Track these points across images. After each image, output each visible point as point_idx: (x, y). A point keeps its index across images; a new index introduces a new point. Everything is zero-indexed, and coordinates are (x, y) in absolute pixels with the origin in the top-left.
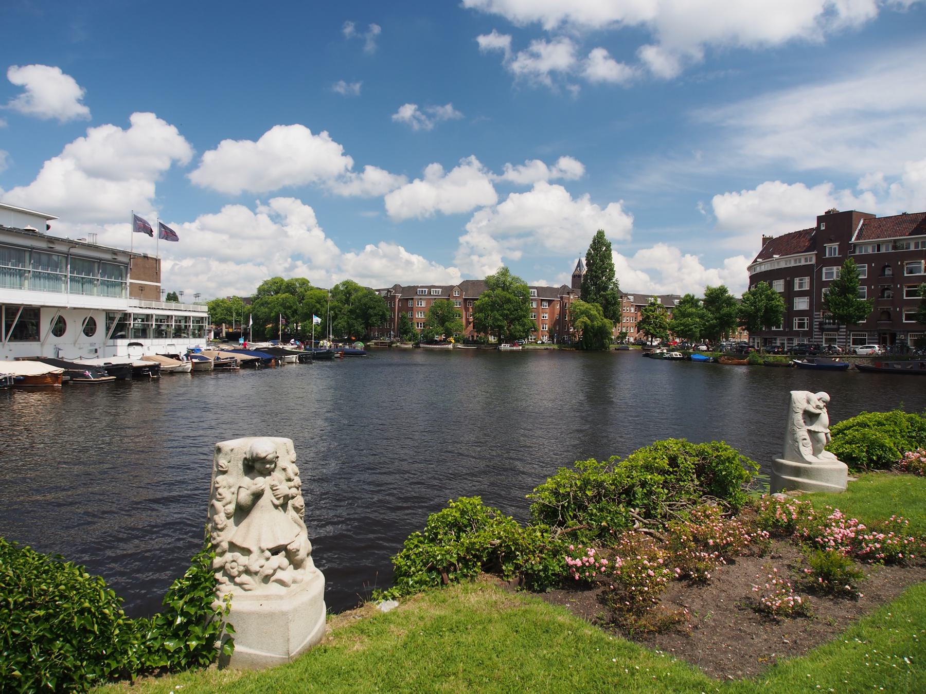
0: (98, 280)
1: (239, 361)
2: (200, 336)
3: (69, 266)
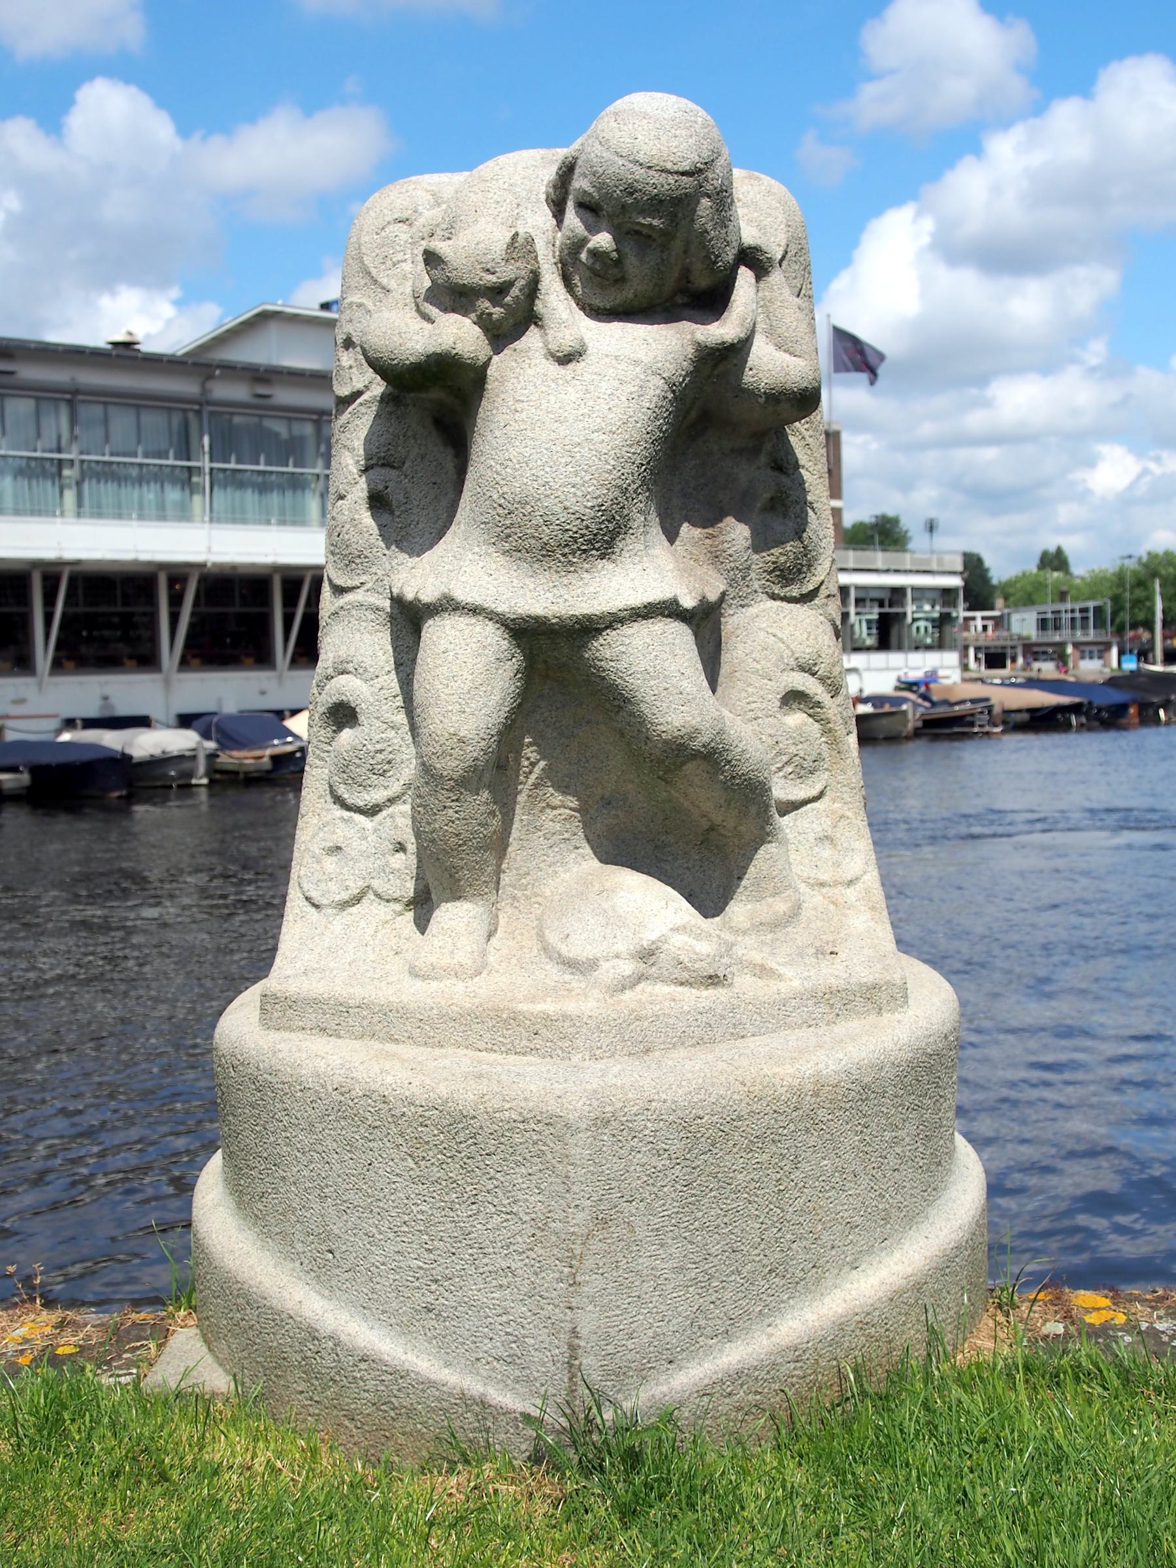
0: (72, 462)
1: (997, 710)
2: (940, 645)
3: (206, 440)
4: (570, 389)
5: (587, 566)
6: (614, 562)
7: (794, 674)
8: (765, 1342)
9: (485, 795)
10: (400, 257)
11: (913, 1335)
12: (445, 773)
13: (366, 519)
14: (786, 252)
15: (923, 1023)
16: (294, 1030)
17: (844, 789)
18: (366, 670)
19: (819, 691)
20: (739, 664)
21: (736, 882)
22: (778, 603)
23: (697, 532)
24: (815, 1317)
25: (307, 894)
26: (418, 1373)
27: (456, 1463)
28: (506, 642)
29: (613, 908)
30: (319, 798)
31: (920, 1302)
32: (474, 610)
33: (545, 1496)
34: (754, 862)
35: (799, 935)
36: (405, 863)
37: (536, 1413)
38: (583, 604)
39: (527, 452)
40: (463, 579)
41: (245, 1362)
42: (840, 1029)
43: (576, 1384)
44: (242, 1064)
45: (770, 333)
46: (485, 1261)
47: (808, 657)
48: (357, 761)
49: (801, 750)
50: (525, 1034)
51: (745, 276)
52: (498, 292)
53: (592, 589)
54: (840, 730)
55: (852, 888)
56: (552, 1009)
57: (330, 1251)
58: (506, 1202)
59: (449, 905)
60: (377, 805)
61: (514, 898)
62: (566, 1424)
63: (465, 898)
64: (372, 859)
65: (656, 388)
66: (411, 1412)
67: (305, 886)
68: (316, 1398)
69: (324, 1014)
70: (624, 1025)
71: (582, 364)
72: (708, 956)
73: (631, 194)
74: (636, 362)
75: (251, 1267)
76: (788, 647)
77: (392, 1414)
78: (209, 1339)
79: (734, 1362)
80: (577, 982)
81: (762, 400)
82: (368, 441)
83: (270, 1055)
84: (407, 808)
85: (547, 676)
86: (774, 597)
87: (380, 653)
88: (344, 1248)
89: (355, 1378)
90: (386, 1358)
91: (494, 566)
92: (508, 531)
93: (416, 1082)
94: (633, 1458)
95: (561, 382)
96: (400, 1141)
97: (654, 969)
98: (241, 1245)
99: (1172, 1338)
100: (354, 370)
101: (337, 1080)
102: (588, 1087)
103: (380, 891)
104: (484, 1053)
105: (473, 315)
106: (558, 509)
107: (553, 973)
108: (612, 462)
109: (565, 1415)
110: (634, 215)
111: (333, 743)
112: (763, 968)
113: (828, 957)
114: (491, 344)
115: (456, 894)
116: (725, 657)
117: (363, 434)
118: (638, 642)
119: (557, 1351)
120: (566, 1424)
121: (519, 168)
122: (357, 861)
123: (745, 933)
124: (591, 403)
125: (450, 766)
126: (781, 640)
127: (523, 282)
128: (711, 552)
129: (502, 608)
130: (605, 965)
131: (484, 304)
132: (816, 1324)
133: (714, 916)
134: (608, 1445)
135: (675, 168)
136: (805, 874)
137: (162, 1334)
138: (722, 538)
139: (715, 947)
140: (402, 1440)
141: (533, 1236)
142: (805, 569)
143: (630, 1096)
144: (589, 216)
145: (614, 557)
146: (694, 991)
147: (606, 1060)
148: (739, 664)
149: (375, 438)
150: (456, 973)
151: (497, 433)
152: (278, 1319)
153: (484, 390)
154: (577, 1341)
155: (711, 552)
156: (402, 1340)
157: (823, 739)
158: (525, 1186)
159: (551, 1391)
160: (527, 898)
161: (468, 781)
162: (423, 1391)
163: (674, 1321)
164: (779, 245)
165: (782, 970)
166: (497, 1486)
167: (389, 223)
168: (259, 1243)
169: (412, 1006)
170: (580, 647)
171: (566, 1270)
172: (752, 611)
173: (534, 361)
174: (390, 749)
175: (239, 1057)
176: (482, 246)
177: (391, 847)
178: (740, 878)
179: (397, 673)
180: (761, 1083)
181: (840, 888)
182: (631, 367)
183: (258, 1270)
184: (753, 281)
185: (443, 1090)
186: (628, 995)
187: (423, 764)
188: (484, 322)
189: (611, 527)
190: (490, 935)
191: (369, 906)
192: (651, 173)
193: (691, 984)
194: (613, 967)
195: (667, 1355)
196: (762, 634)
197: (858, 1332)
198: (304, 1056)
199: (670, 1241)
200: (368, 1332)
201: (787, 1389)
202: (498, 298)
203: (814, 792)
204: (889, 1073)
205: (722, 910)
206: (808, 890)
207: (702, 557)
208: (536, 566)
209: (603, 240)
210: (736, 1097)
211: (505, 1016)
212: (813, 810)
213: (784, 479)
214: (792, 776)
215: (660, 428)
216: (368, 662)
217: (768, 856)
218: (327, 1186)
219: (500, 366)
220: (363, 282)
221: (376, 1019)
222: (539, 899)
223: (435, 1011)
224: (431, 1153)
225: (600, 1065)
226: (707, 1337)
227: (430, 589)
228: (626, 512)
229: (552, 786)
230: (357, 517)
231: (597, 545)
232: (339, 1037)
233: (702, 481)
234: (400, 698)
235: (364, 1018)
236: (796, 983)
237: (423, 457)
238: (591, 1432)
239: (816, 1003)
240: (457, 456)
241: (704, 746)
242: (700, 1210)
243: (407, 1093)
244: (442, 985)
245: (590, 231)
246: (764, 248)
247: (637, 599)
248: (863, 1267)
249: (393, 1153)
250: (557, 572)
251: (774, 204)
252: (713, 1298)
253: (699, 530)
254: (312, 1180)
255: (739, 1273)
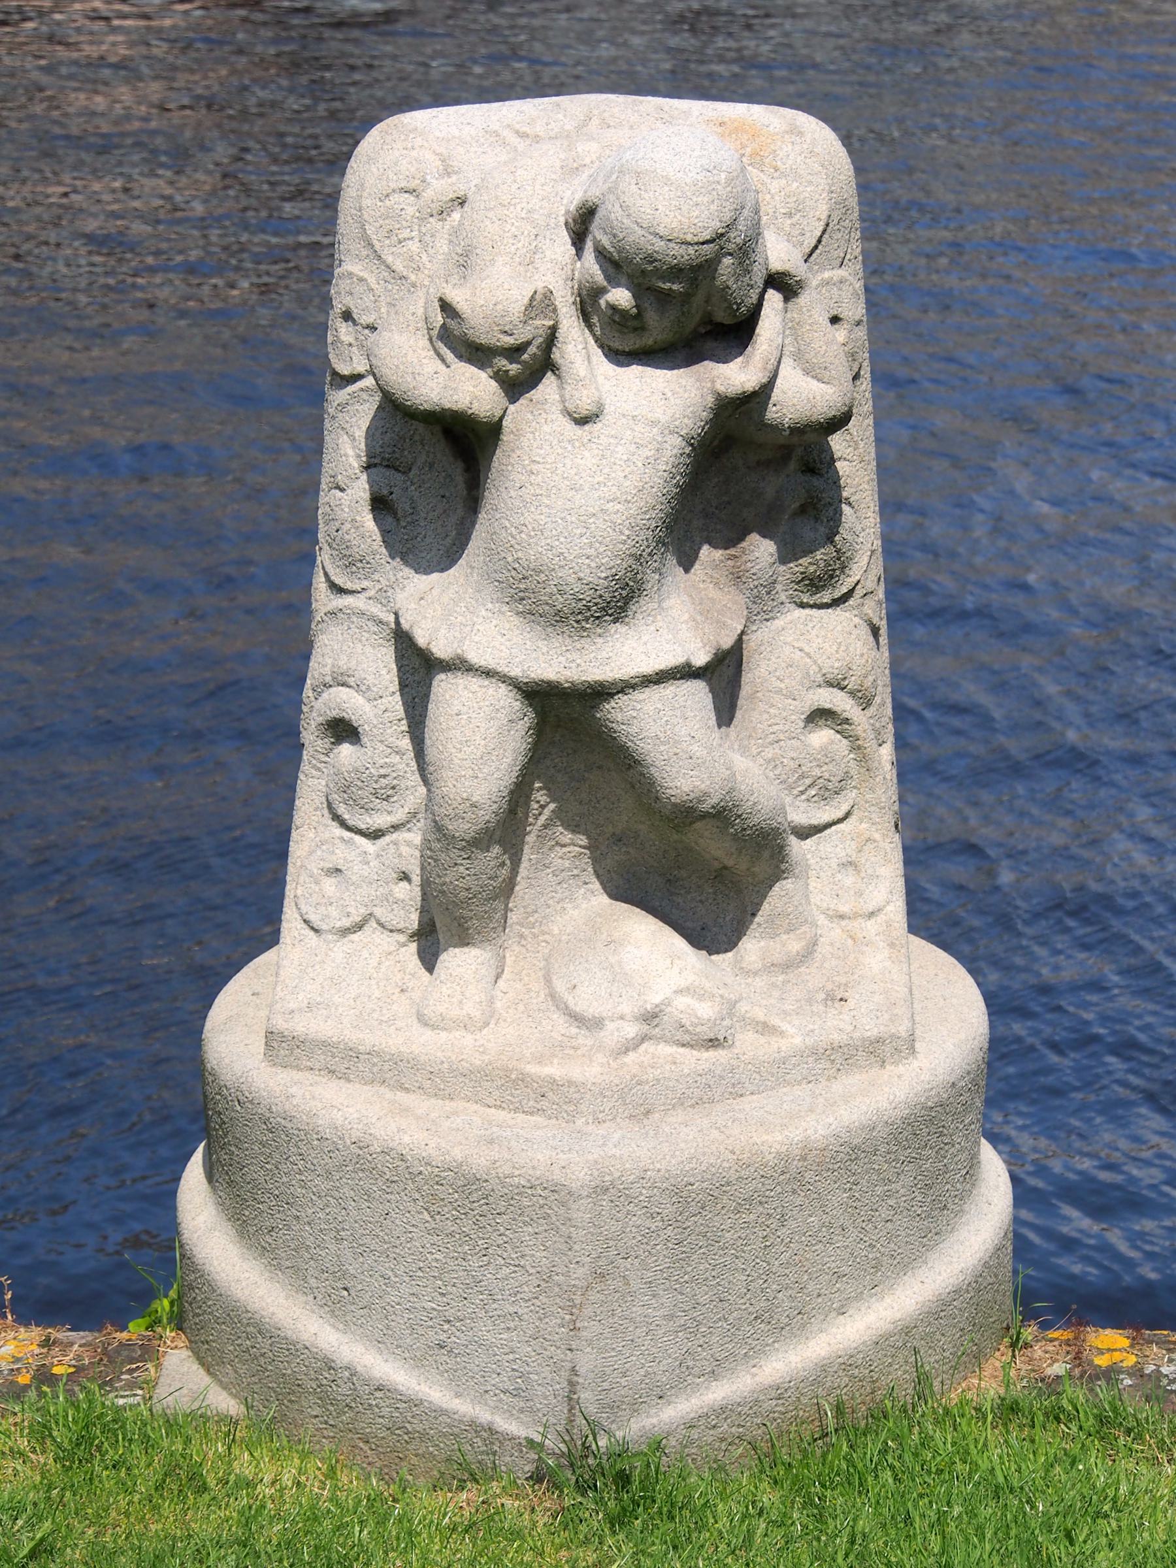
4: (587, 454)
5: (599, 631)
6: (627, 624)
7: (821, 690)
8: (749, 1381)
9: (496, 850)
10: (406, 234)
11: (901, 1375)
12: (457, 835)
13: (368, 522)
14: (827, 225)
15: (925, 1076)
16: (301, 1070)
17: (873, 809)
18: (369, 688)
19: (848, 707)
20: (762, 683)
21: (749, 917)
22: (808, 611)
23: (718, 554)
24: (799, 1359)
25: (305, 917)
26: (431, 1402)
27: (465, 1481)
28: (518, 703)
29: (620, 962)
30: (316, 809)
31: (909, 1345)
32: (488, 673)
33: (547, 1510)
34: (768, 899)
35: (813, 977)
36: (409, 893)
37: (538, 1438)
38: (595, 670)
39: (543, 519)
40: (477, 639)
41: (255, 1387)
42: (837, 1087)
43: (574, 1415)
44: (251, 1102)
45: (798, 356)
46: (495, 1306)
47: (836, 672)
48: (359, 783)
49: (825, 771)
50: (533, 1096)
51: (773, 298)
52: (514, 352)
53: (604, 655)
54: (870, 744)
55: (873, 920)
56: (558, 1073)
57: (345, 1289)
58: (514, 1256)
59: (457, 950)
60: (380, 830)
61: (522, 936)
62: (565, 1449)
63: (473, 944)
64: (374, 885)
65: (673, 449)
66: (423, 1436)
67: (304, 909)
68: (332, 1422)
69: (333, 1056)
70: (626, 1090)
71: (599, 425)
72: (709, 1020)
73: (652, 262)
74: (654, 423)
75: (262, 1298)
76: (815, 662)
77: (406, 1437)
78: (207, 1358)
79: (719, 1398)
80: (584, 1039)
81: (788, 432)
82: (370, 434)
83: (283, 1098)
84: (416, 837)
85: (559, 726)
86: (802, 605)
87: (384, 672)
88: (360, 1287)
89: (370, 1405)
90: (401, 1388)
91: (507, 626)
92: (521, 594)
93: (432, 1144)
94: (623, 1479)
95: (577, 444)
96: (417, 1196)
97: (657, 1030)
98: (247, 1275)
99: (1171, 1382)
100: (354, 349)
101: (356, 1135)
102: (590, 1157)
103: (383, 920)
104: (493, 1110)
105: (489, 370)
106: (571, 579)
107: (559, 1025)
108: (627, 532)
109: (565, 1442)
110: (654, 280)
111: (332, 755)
112: (765, 1025)
113: (837, 1004)
114: (507, 395)
115: (464, 940)
116: (746, 678)
117: (365, 423)
118: (649, 708)
119: (558, 1386)
120: (565, 1449)
121: (538, 187)
122: (359, 887)
123: (756, 974)
124: (606, 471)
125: (463, 828)
126: (808, 655)
127: (540, 340)
128: (732, 573)
129: (515, 672)
130: (610, 1026)
131: (502, 363)
132: (799, 1366)
133: (726, 951)
134: (602, 1468)
135: (696, 239)
136: (825, 905)
137: (149, 1352)
138: (745, 558)
139: (717, 1009)
140: (415, 1460)
141: (539, 1286)
142: (838, 572)
143: (627, 1166)
144: (611, 270)
145: (627, 620)
146: (694, 1052)
147: (608, 1124)
148: (762, 683)
149: (378, 434)
150: (466, 1025)
151: (513, 493)
152: (293, 1348)
153: (499, 439)
154: (576, 1378)
155: (732, 573)
156: (416, 1372)
157: (852, 756)
158: (531, 1243)
159: (553, 1420)
160: (535, 936)
161: (480, 841)
162: (435, 1418)
163: (665, 1362)
164: (819, 219)
165: (785, 1026)
166: (503, 1500)
167: (394, 191)
168: (267, 1274)
169: (423, 1058)
170: (593, 707)
171: (568, 1317)
172: (778, 623)
173: (550, 417)
174: (395, 775)
175: (247, 1094)
176: (499, 307)
177: (395, 876)
178: (754, 915)
179: (402, 695)
180: (750, 1151)
181: (860, 920)
182: (648, 428)
183: (269, 1301)
184: (781, 305)
185: (458, 1153)
186: (632, 1055)
187: (435, 822)
188: (500, 377)
189: (624, 593)
190: (498, 977)
191: (371, 936)
192: (672, 245)
193: (692, 1046)
194: (618, 1029)
195: (658, 1391)
196: (787, 650)
197: (840, 1373)
198: (320, 1105)
199: (661, 1292)
200: (383, 1364)
201: (768, 1424)
202: (515, 355)
203: (840, 814)
204: (882, 1132)
205: (736, 945)
206: (826, 922)
207: (723, 580)
208: (549, 630)
209: (621, 296)
210: (725, 1165)
211: (513, 1076)
212: (837, 832)
213: (816, 482)
214: (816, 799)
215: (677, 485)
216: (371, 679)
217: (783, 893)
218: (343, 1229)
219: (518, 416)
220: (365, 253)
221: (386, 1067)
222: (547, 937)
223: (446, 1066)
224: (446, 1209)
225: (601, 1131)
226: (695, 1376)
227: (442, 642)
228: (639, 577)
229: (562, 825)
230: (358, 518)
231: (610, 612)
232: (349, 1081)
233: (725, 499)
234: (404, 722)
235: (374, 1065)
236: (798, 1040)
237: (431, 466)
238: (587, 1457)
239: (816, 1060)
240: (467, 470)
241: (713, 807)
242: (689, 1265)
243: (424, 1154)
244: (451, 1036)
245: (609, 282)
246: (793, 271)
247: (649, 666)
248: (850, 1312)
249: (410, 1206)
250: (570, 636)
251: (817, 167)
252: (701, 1342)
253: (721, 552)
254: (328, 1222)
255: (726, 1320)
